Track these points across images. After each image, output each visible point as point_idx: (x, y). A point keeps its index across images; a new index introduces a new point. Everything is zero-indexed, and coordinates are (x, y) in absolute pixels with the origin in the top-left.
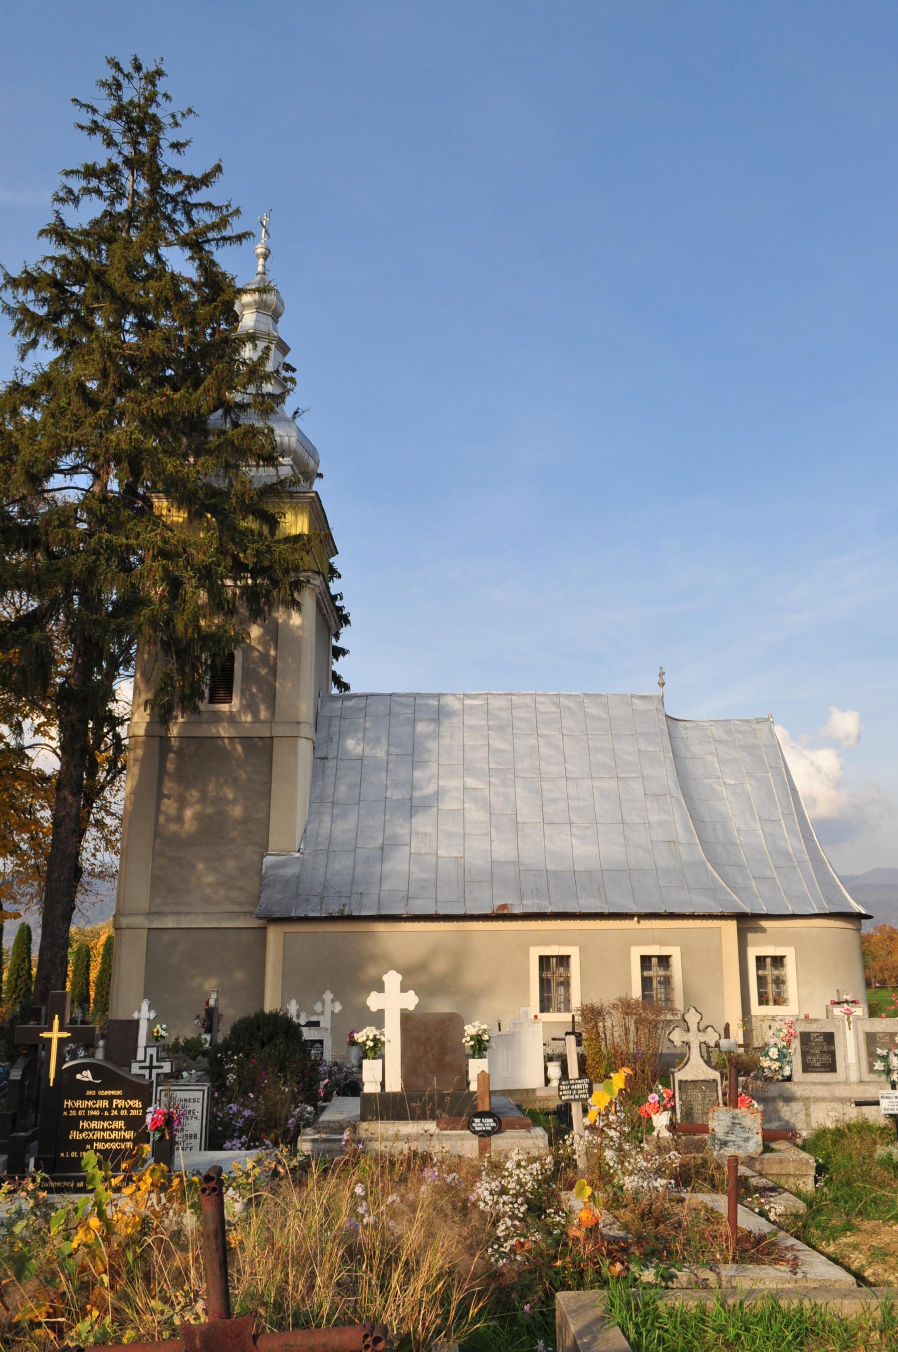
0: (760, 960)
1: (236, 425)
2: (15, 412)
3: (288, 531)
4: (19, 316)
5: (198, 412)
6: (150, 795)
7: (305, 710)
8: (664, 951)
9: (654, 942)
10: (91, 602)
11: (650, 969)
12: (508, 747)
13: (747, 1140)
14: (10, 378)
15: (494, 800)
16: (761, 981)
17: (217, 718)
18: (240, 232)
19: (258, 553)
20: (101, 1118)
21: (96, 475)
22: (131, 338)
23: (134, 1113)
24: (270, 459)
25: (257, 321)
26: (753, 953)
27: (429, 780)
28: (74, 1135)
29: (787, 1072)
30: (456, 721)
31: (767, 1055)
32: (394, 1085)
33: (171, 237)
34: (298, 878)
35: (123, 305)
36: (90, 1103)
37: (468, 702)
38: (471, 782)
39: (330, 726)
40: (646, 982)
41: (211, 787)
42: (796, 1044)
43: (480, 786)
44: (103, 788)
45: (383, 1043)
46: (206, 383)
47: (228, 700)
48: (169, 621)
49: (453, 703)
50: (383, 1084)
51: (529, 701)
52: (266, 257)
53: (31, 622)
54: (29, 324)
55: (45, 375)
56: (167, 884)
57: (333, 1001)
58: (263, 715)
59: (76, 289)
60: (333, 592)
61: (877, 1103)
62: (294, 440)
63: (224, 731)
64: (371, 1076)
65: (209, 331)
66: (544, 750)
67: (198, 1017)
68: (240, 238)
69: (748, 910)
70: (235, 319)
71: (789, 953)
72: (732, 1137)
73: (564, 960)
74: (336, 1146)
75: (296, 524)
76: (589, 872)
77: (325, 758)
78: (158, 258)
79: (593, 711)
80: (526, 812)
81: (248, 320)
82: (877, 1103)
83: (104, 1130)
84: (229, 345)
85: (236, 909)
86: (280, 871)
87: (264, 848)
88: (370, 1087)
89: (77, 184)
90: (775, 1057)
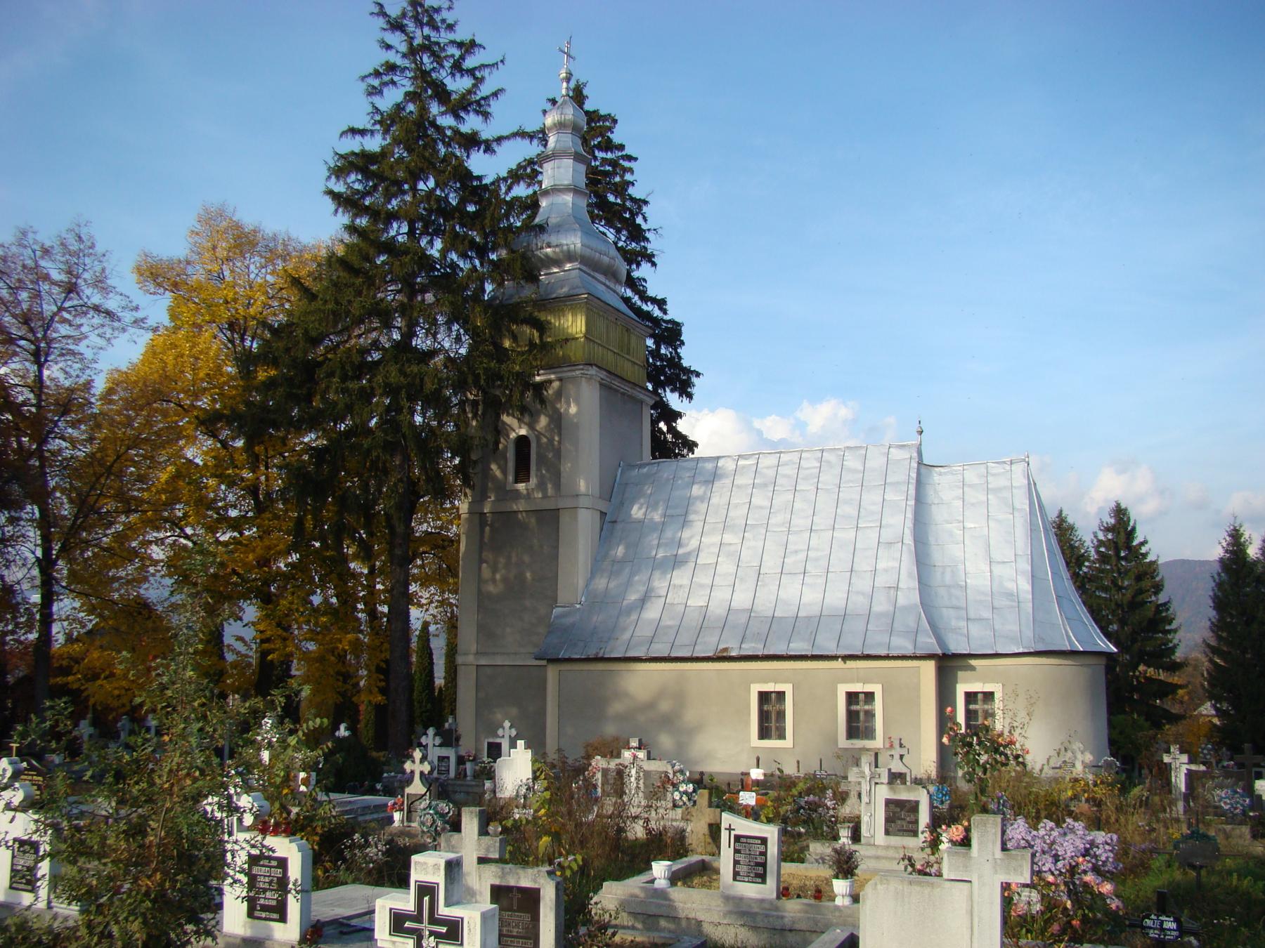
17: (516, 495)
26: (961, 689)
27: (692, 537)
30: (728, 481)
37: (741, 462)
40: (852, 716)
41: (514, 555)
47: (527, 480)
57: (511, 727)
58: (550, 491)
63: (520, 506)
73: (870, 696)
89: (376, 82)
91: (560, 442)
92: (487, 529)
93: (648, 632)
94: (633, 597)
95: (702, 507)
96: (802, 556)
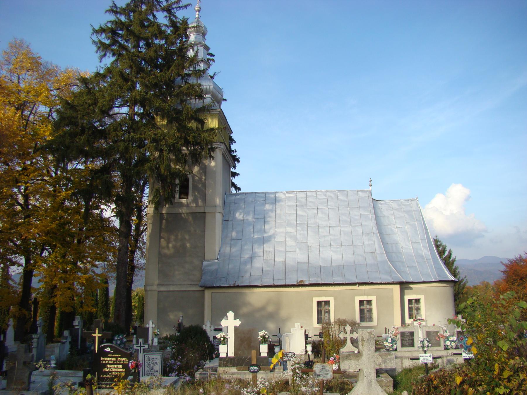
0: (410, 301)
1: (186, 82)
2: (98, 84)
3: (209, 126)
4: (99, 45)
5: (169, 79)
6: (157, 236)
7: (218, 201)
8: (369, 298)
9: (365, 295)
10: (128, 161)
11: (412, 304)
12: (304, 214)
13: (327, 374)
14: (95, 70)
15: (299, 237)
16: (410, 309)
17: (181, 205)
18: (186, 4)
19: (194, 137)
20: (114, 364)
21: (131, 108)
22: (143, 50)
23: (125, 362)
24: (200, 97)
25: (196, 38)
26: (407, 298)
27: (271, 228)
28: (105, 369)
29: (395, 347)
30: (283, 203)
31: (387, 341)
32: (231, 354)
33: (159, 8)
34: (217, 270)
35: (138, 38)
36: (110, 359)
38: (289, 229)
39: (230, 207)
40: (362, 311)
41: (179, 234)
42: (399, 336)
43: (293, 231)
44: (142, 233)
45: (227, 339)
46: (172, 68)
47: (187, 197)
48: (158, 169)
49: (281, 196)
50: (227, 354)
51: (314, 194)
52: (199, 11)
53: (106, 170)
54: (103, 47)
55: (108, 69)
56: (164, 275)
59: (120, 32)
60: (233, 148)
61: (419, 359)
62: (212, 87)
63: (184, 210)
64: (223, 350)
65: (179, 41)
66: (320, 215)
67: (174, 326)
68: (186, 6)
69: (404, 280)
70: (187, 37)
71: (422, 297)
72: (322, 373)
74: (205, 376)
75: (213, 123)
76: (338, 266)
77: (228, 220)
78: (154, 16)
79: (341, 197)
80: (312, 241)
81: (192, 38)
82: (419, 359)
83: (115, 368)
84: (182, 50)
85: (193, 283)
86: (209, 268)
87: (203, 259)
88: (223, 355)
90: (390, 342)
91: (205, 179)
92: (164, 221)
93: (259, 273)
94: (246, 256)
95: (272, 215)
96: (327, 238)
